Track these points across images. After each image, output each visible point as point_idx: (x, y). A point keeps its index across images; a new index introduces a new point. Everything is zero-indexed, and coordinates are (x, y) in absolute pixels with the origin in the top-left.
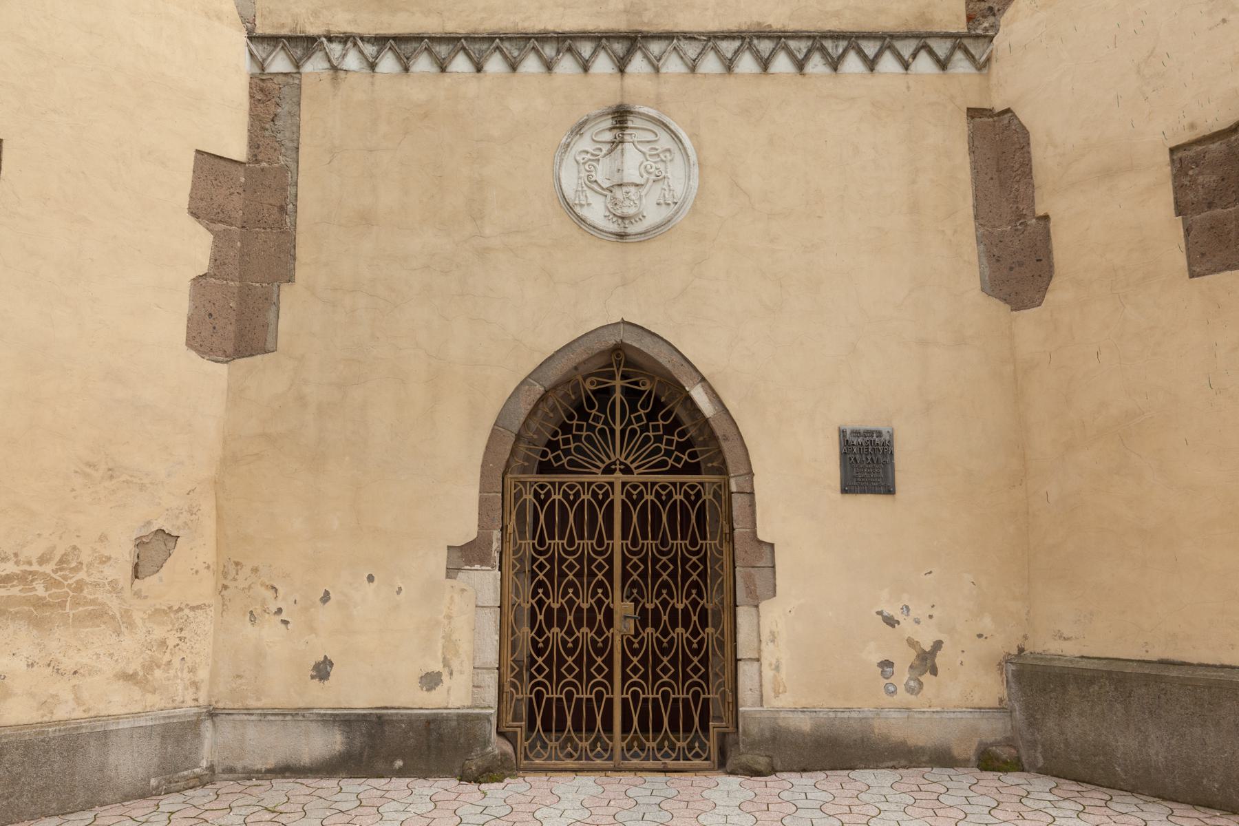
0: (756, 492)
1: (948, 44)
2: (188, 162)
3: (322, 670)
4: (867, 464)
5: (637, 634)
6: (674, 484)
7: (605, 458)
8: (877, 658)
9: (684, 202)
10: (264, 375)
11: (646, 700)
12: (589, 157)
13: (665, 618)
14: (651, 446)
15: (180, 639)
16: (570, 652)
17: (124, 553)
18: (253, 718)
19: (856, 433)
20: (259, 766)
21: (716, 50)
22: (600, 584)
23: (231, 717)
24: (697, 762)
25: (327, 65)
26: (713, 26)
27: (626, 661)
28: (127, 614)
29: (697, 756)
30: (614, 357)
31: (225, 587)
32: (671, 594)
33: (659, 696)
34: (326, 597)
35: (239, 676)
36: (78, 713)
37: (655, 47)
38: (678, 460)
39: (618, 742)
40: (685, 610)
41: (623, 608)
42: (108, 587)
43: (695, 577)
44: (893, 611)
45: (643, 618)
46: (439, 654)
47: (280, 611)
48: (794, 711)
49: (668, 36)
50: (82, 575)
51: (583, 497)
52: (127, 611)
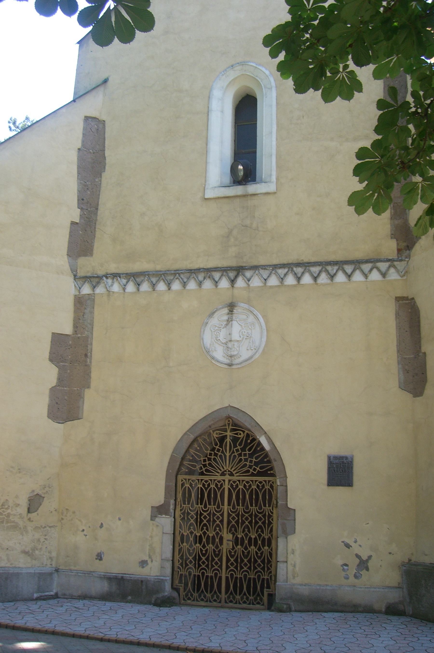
0: (288, 486)
1: (387, 264)
2: (48, 338)
3: (100, 557)
4: (340, 472)
5: (233, 548)
6: (252, 481)
7: (221, 468)
8: (341, 562)
9: (259, 349)
10: (78, 429)
11: (236, 578)
12: (217, 328)
13: (246, 542)
14: (243, 463)
15: (45, 539)
16: (204, 555)
17: (24, 502)
18: (73, 574)
19: (335, 458)
20: (75, 594)
21: (276, 273)
22: (218, 525)
23: (65, 573)
24: (258, 606)
25: (105, 290)
26: (275, 261)
27: (228, 560)
28: (25, 527)
29: (258, 603)
30: (227, 422)
31: (62, 519)
32: (249, 531)
33: (242, 576)
34: (102, 526)
35: (68, 556)
36: (8, 565)
37: (248, 274)
38: (255, 470)
39: (223, 596)
40: (255, 538)
41: (227, 536)
42: (18, 516)
43: (260, 523)
44: (350, 541)
45: (236, 541)
46: (147, 553)
47: (83, 530)
48: (301, 585)
49: (255, 268)
50: (9, 511)
51: (211, 486)
52: (25, 526)
